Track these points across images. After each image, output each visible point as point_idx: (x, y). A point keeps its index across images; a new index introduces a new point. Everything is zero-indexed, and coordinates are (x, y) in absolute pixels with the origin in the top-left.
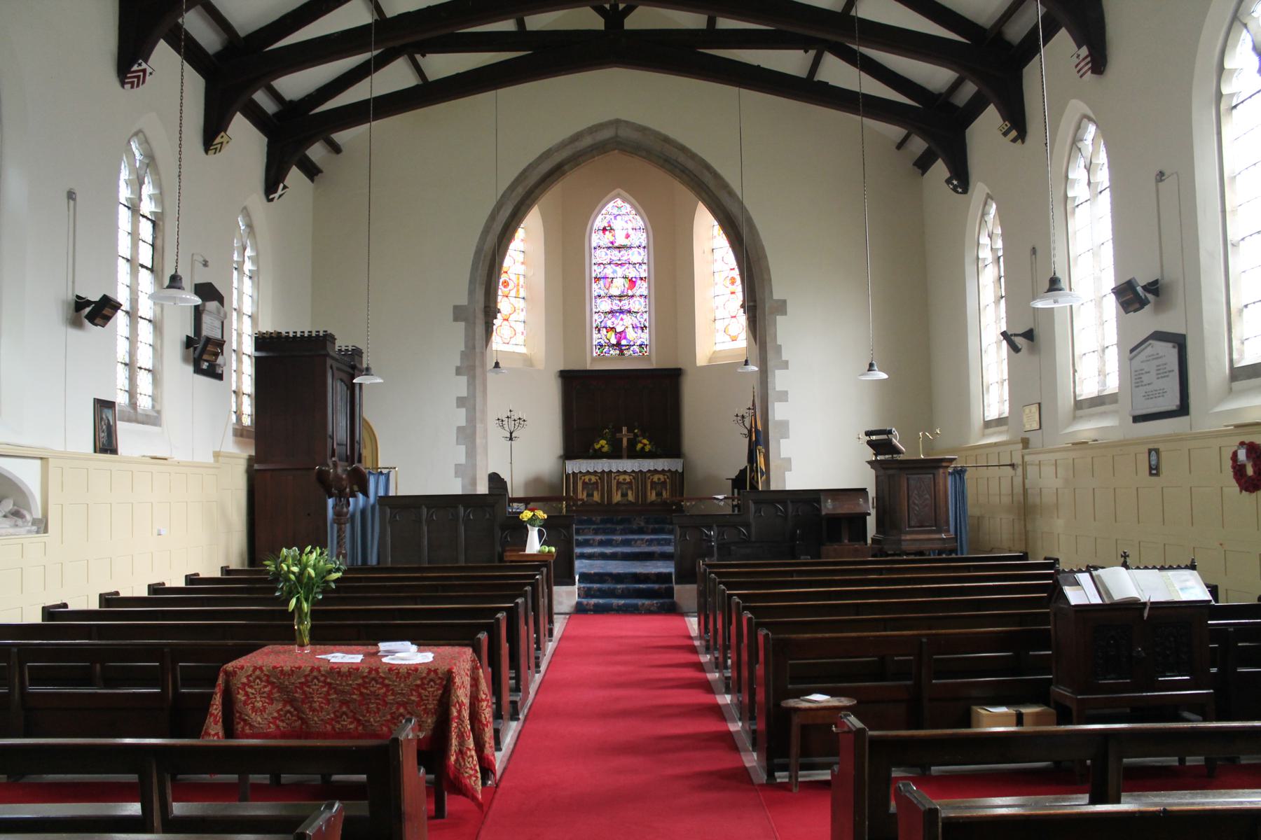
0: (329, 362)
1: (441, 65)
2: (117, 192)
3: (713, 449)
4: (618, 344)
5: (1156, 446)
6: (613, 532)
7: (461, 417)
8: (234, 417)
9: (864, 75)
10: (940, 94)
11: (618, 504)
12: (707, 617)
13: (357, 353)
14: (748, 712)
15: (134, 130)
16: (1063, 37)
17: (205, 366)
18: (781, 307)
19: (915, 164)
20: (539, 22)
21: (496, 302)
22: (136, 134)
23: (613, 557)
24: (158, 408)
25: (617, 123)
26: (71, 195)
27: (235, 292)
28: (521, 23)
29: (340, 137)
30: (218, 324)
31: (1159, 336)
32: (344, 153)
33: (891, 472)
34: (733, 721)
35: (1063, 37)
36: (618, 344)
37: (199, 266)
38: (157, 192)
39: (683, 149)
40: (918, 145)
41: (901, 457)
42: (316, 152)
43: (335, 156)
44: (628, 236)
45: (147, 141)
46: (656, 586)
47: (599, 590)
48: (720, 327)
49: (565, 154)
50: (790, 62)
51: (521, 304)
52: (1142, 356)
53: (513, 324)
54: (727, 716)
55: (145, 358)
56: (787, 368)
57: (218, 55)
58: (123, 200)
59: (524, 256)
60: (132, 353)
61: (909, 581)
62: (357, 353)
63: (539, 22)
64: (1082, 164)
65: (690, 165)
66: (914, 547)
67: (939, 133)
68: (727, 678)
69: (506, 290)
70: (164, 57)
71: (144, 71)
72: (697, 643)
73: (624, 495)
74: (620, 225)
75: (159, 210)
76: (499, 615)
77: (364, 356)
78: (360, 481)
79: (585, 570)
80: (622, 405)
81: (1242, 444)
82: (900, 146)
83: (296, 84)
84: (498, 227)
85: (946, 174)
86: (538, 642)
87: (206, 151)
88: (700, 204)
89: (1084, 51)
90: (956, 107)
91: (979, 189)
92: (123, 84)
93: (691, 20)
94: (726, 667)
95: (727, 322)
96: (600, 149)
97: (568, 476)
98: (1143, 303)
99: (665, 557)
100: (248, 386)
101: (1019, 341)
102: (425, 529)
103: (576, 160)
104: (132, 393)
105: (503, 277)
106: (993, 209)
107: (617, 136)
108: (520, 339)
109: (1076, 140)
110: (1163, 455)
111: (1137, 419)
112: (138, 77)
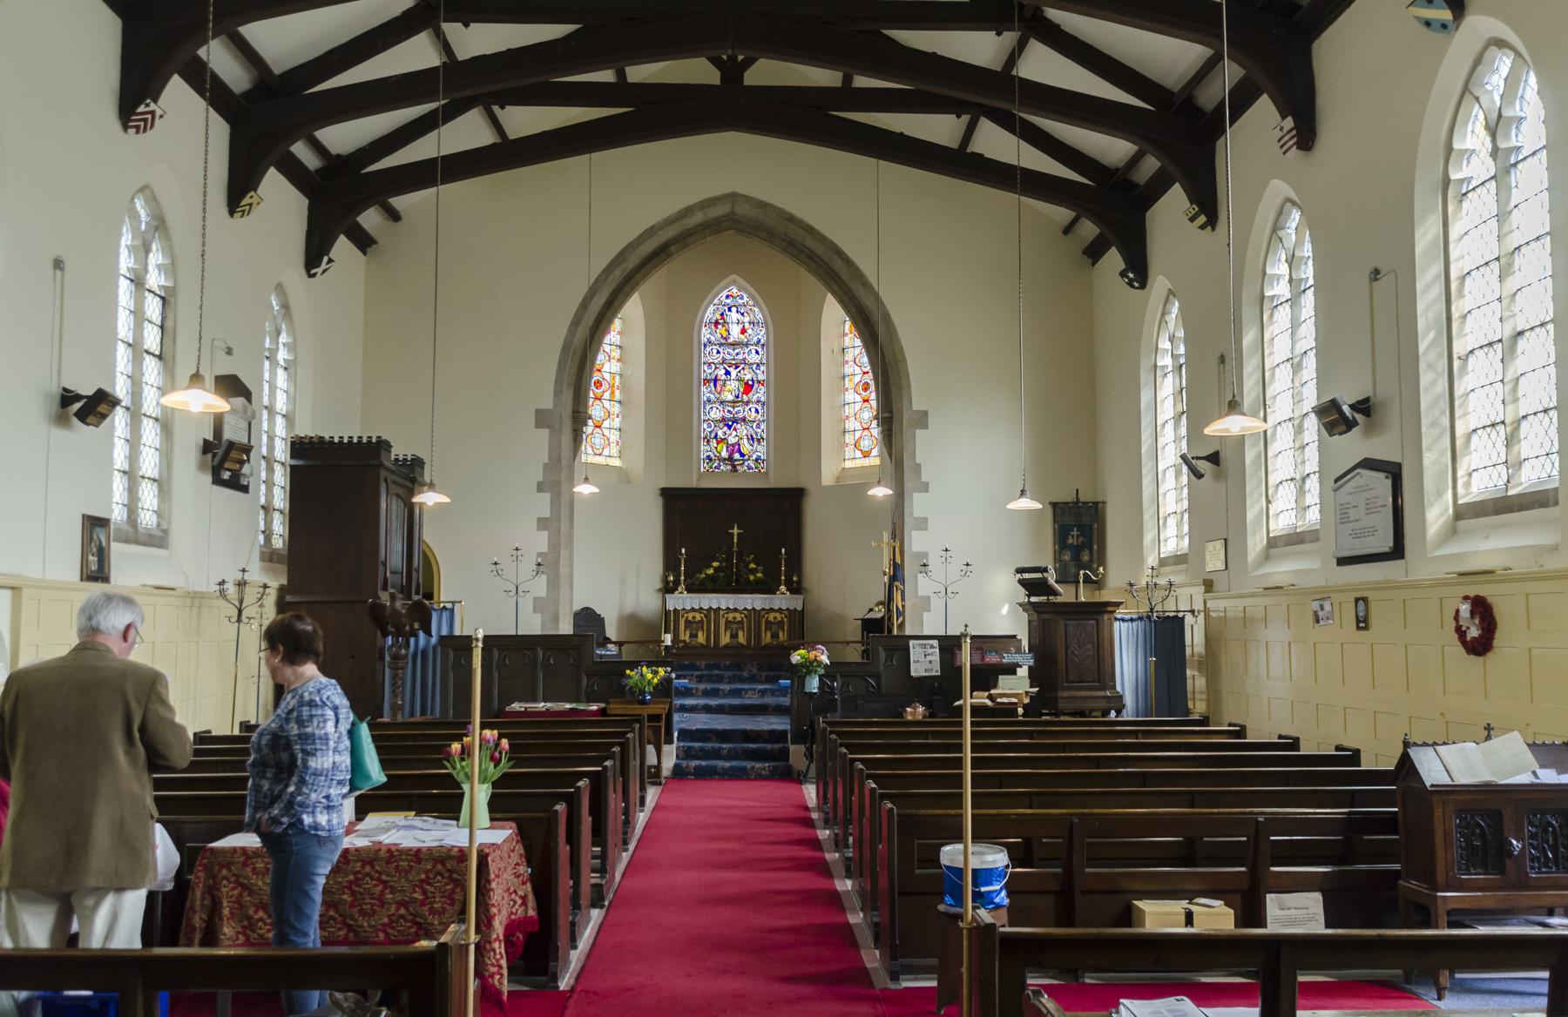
0: (383, 474)
1: (524, 120)
2: (117, 262)
3: (841, 581)
4: (731, 459)
5: (1364, 594)
6: (720, 679)
7: (541, 542)
8: (261, 538)
9: (1023, 144)
10: (1117, 170)
11: (726, 646)
12: (826, 785)
13: (417, 463)
14: (869, 901)
15: (140, 185)
16: (1264, 107)
17: (226, 475)
18: (922, 420)
19: (1084, 252)
20: (639, 73)
21: (586, 407)
22: (142, 190)
23: (720, 710)
24: (164, 526)
25: (733, 197)
26: (58, 264)
27: (266, 387)
28: (621, 74)
29: (398, 202)
30: (244, 425)
31: (1369, 464)
32: (404, 220)
33: (1046, 616)
34: (854, 911)
35: (1264, 107)
36: (731, 459)
37: (220, 354)
38: (168, 261)
39: (810, 230)
40: (1089, 230)
41: (1059, 599)
42: (370, 219)
43: (392, 224)
44: (743, 331)
45: (155, 199)
46: (769, 746)
47: (702, 749)
48: (850, 437)
49: (672, 232)
50: (939, 128)
51: (616, 409)
52: (1349, 487)
53: (606, 432)
54: (846, 904)
55: (149, 463)
56: (927, 490)
57: (246, 94)
58: (123, 270)
59: (620, 354)
60: (133, 457)
61: (1064, 747)
62: (417, 463)
63: (639, 73)
64: (1283, 257)
65: (819, 249)
66: (1072, 706)
67: (1113, 216)
68: (848, 859)
69: (599, 391)
70: (178, 95)
71: (153, 113)
72: (815, 815)
73: (734, 636)
74: (735, 318)
75: (170, 284)
76: (580, 784)
77: (427, 467)
78: (422, 616)
79: (684, 726)
80: (734, 530)
81: (1466, 598)
82: (1067, 230)
83: (344, 136)
84: (589, 318)
85: (1121, 265)
86: (626, 812)
87: (232, 213)
88: (829, 295)
89: (1289, 123)
90: (1128, 193)
91: (1159, 283)
92: (126, 128)
93: (823, 77)
94: (847, 846)
95: (858, 435)
96: (713, 227)
97: (667, 613)
98: (1350, 425)
99: (779, 710)
100: (280, 499)
101: (1203, 466)
102: (496, 675)
103: (683, 240)
104: (132, 507)
105: (596, 377)
106: (1175, 308)
107: (733, 213)
108: (614, 450)
109: (1277, 227)
110: (1373, 607)
111: (1342, 561)
112: (145, 120)
